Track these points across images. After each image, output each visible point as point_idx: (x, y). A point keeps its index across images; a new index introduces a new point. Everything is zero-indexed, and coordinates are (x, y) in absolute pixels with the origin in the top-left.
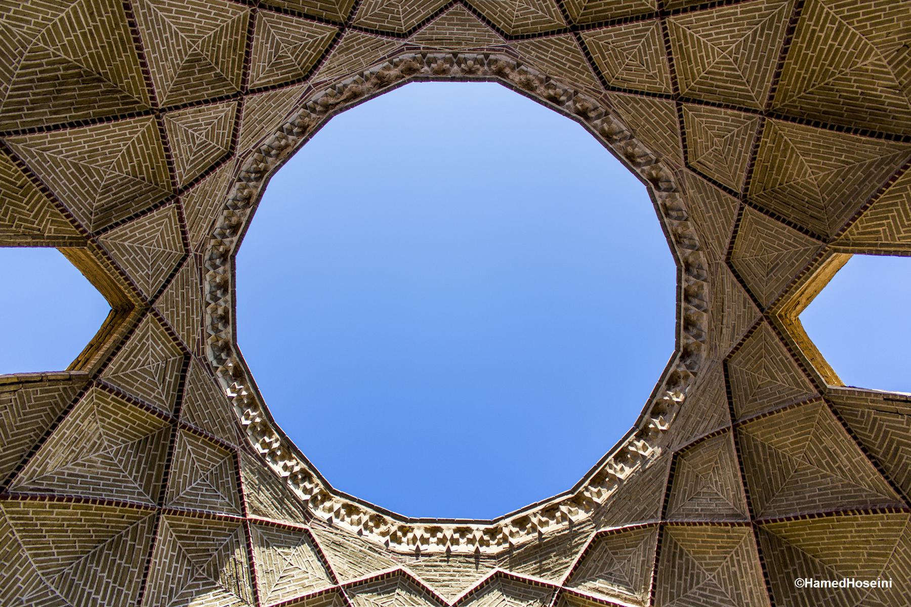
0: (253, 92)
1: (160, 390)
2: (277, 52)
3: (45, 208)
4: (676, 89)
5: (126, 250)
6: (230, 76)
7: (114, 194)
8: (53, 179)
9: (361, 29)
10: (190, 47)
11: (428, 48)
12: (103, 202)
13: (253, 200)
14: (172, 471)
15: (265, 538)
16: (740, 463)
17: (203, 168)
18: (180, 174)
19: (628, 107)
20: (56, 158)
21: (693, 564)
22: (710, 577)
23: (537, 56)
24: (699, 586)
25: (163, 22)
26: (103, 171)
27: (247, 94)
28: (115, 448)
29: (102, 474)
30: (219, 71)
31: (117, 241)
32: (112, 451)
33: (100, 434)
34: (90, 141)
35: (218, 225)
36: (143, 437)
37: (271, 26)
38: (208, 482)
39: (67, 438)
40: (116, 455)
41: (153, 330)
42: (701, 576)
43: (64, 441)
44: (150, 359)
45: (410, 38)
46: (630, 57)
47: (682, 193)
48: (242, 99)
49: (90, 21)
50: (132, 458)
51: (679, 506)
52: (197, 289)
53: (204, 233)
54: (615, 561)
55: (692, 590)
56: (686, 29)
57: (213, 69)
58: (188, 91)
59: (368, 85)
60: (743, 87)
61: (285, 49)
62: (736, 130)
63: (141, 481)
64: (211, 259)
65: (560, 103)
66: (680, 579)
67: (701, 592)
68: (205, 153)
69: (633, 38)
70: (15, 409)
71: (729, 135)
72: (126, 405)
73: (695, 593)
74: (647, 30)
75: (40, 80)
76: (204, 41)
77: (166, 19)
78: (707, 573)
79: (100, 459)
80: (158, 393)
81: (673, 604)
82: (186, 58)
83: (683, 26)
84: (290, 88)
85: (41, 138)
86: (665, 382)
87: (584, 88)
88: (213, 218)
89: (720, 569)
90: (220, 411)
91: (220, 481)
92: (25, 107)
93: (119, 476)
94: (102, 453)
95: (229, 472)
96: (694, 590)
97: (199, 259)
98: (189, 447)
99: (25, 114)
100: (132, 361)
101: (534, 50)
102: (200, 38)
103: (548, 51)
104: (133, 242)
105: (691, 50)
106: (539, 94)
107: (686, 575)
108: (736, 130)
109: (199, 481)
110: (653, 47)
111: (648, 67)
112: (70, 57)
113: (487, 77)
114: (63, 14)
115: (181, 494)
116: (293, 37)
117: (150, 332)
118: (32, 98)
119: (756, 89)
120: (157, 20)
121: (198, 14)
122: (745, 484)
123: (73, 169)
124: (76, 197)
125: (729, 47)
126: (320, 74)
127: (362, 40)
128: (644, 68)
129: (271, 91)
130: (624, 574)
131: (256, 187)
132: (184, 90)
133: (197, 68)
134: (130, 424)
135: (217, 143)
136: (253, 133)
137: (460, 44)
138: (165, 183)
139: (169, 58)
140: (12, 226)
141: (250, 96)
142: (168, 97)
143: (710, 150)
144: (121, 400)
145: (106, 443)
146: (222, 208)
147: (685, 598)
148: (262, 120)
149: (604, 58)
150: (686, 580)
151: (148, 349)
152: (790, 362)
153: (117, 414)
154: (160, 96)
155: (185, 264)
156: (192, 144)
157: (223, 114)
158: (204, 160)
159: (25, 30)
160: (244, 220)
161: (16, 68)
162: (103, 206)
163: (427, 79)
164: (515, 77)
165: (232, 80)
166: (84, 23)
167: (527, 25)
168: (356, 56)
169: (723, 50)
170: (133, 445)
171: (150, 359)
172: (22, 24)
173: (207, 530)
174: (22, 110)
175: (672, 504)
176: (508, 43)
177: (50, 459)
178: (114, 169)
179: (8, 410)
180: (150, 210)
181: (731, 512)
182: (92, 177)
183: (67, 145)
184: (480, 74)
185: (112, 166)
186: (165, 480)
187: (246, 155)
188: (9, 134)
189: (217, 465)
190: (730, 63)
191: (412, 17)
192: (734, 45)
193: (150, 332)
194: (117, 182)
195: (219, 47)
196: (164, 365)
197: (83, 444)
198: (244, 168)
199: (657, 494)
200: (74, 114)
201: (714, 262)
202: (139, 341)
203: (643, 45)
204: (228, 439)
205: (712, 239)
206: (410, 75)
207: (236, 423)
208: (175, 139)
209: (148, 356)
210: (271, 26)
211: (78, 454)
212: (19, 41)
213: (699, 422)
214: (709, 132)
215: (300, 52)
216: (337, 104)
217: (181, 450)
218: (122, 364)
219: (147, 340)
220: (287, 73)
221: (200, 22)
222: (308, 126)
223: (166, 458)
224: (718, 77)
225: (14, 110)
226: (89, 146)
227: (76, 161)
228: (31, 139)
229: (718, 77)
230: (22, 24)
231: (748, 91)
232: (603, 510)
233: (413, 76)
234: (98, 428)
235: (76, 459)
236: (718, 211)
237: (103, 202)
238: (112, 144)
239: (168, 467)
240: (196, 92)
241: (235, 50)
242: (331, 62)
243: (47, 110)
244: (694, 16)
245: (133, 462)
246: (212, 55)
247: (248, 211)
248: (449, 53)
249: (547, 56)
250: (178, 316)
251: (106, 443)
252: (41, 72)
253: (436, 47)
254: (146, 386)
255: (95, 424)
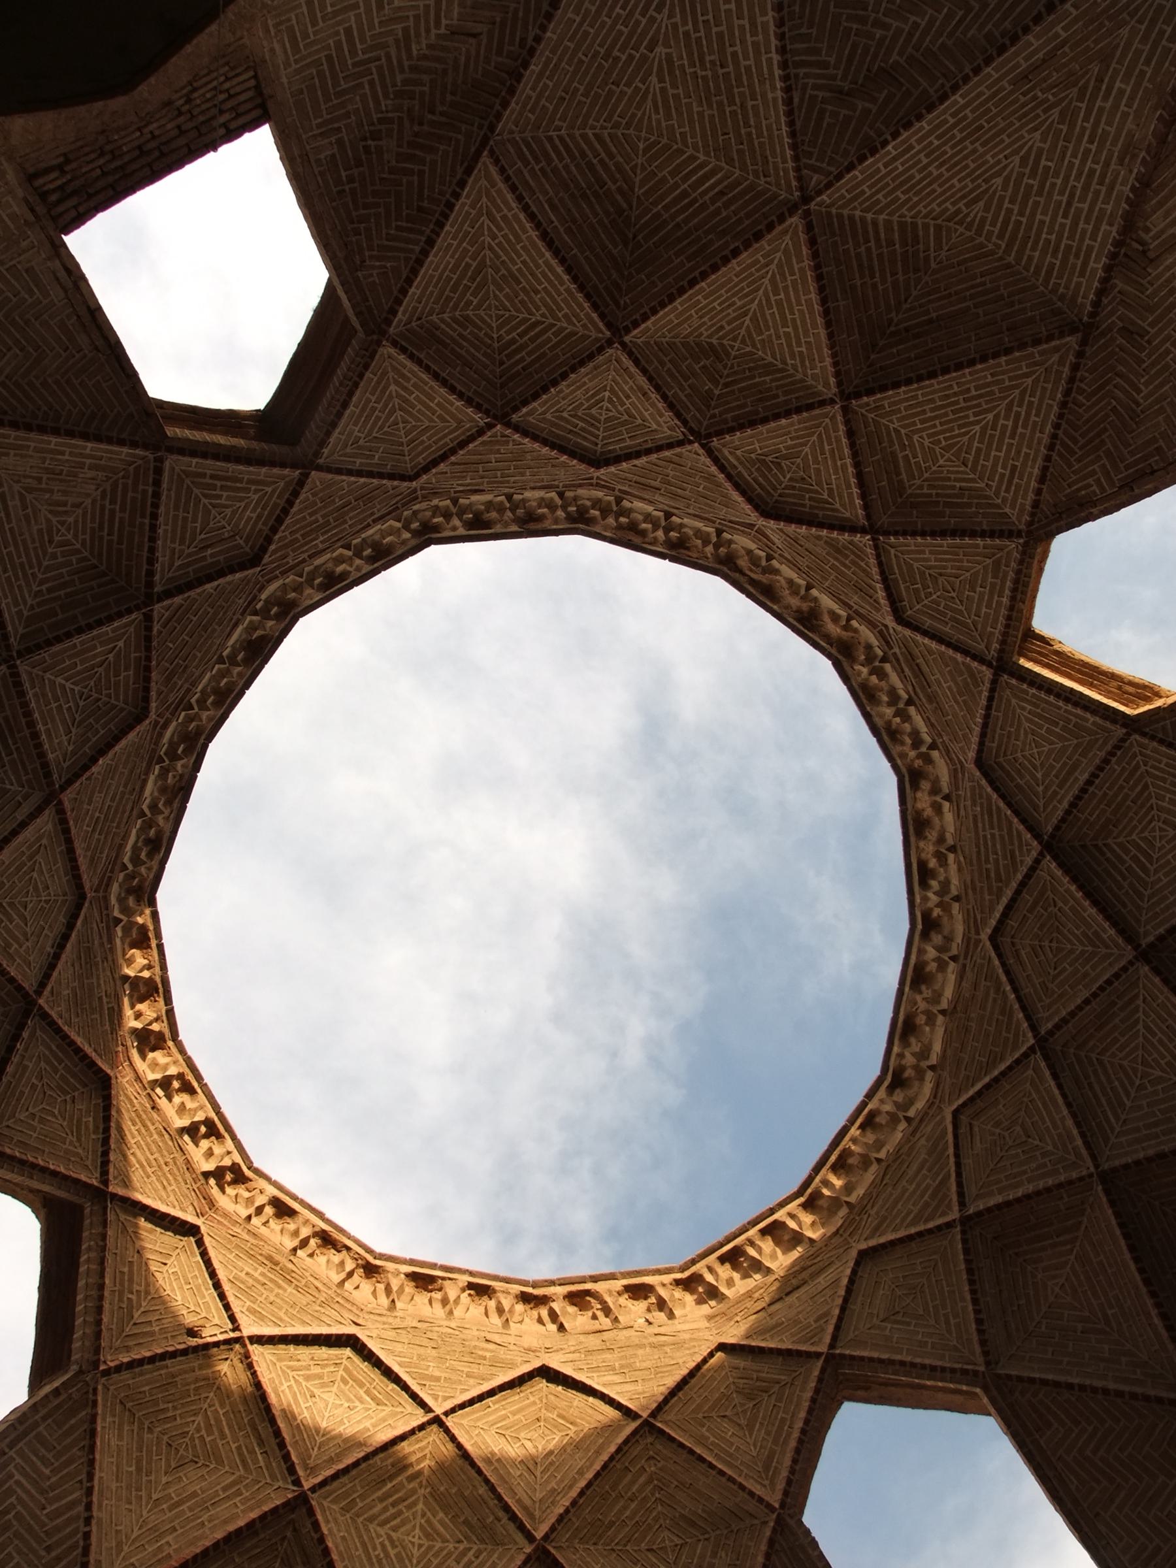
0: (710, 452)
1: (187, 551)
2: (785, 457)
3: (402, 255)
4: (1051, 1033)
5: (383, 391)
6: (716, 411)
7: (460, 335)
8: (450, 245)
9: (878, 556)
10: (735, 339)
11: (898, 660)
12: (443, 326)
13: (533, 526)
14: (76, 640)
15: (44, 841)
16: (605, 1466)
17: (558, 436)
18: (535, 409)
19: (983, 983)
20: (483, 235)
21: (415, 1504)
22: (416, 1540)
23: (975, 817)
24: (393, 1534)
25: (757, 290)
26: (490, 305)
27: (703, 446)
28: (70, 537)
29: (24, 541)
30: (717, 392)
31: (391, 374)
32: (63, 535)
33: (82, 503)
34: (528, 268)
35: (475, 498)
36: (103, 567)
37: (820, 434)
38: (81, 703)
39: (57, 460)
40: (62, 544)
41: (274, 491)
42: (408, 1527)
43: (51, 459)
44: (228, 511)
45: (899, 628)
46: (1054, 945)
47: (911, 1129)
48: (691, 442)
49: (711, 194)
50: (64, 570)
51: (479, 1424)
52: (364, 519)
53: (456, 485)
54: (334, 1389)
55: (378, 1529)
56: (1141, 997)
57: (716, 383)
58: (669, 365)
59: (794, 602)
60: (1113, 1120)
61: (794, 468)
62: (1050, 1148)
63: (39, 604)
64: (415, 513)
65: (924, 884)
66: (382, 1499)
67: (387, 1543)
68: (583, 429)
69: (1085, 934)
70: (71, 362)
71: (1037, 1142)
72: (143, 516)
73: (379, 1536)
74: (1107, 947)
75: (590, 166)
76: (751, 354)
77: (761, 292)
78: (417, 1531)
79: (44, 526)
80: (182, 551)
81: (343, 1515)
82: (714, 341)
83: (1142, 991)
84: (740, 499)
85: (506, 203)
86: (625, 1282)
87: (970, 907)
88: (485, 487)
89: (438, 1545)
90: (195, 656)
91: (91, 720)
92: (543, 163)
93: (31, 567)
94: (55, 523)
95: (112, 726)
96: (381, 1531)
97: (413, 498)
98: (121, 644)
99: (533, 168)
100: (214, 487)
101: (982, 807)
102: (754, 346)
103: (992, 828)
104: (398, 396)
105: (1117, 1021)
106: (918, 848)
107: (393, 1505)
108: (1050, 1148)
109: (76, 689)
110: (1088, 967)
111: (1055, 977)
112: (640, 188)
113: (899, 762)
114: (702, 158)
115: (48, 675)
116: (818, 471)
117: (269, 489)
118: (560, 166)
119: (1123, 1139)
120: (754, 282)
121: (790, 330)
122: (582, 1493)
123: (474, 264)
124: (435, 286)
125: (1152, 1067)
126: (781, 530)
127: (862, 564)
128: (1052, 972)
129: (722, 476)
130: (327, 1415)
131: (556, 521)
132: (666, 359)
133: (707, 363)
134: (115, 538)
135: (604, 438)
136: (642, 480)
137: (930, 700)
138: (510, 396)
139: (706, 319)
140: (352, 222)
141: (701, 451)
142: (647, 343)
143: (998, 1131)
144: (149, 503)
145: (71, 520)
146: (507, 490)
147: (361, 1526)
148: (669, 483)
149: (1030, 911)
150: (385, 1509)
151: (241, 500)
152: (789, 1435)
153: (123, 510)
154: (643, 333)
155: (396, 483)
156: (586, 405)
157: (655, 426)
158: (571, 432)
159: (654, 117)
160: (498, 529)
161: (593, 128)
162: (437, 329)
163: (845, 678)
164: (923, 801)
165: (714, 416)
166: (703, 188)
167: (1012, 780)
168: (833, 567)
169: (1144, 1063)
170: (85, 559)
171: (228, 511)
172: (661, 111)
173: (13, 747)
174: (538, 162)
175: (473, 1412)
176: (971, 766)
177: (15, 455)
178: (499, 317)
179: (64, 355)
180: (461, 396)
181: (528, 1502)
182: (474, 295)
183: (509, 241)
184: (896, 750)
185: (501, 313)
186: (59, 640)
187: (604, 486)
188: (497, 161)
189: (113, 701)
190: (1132, 1084)
191: (932, 617)
192: (1161, 1073)
193: (269, 489)
194: (480, 329)
195: (754, 377)
196: (226, 535)
197: (56, 488)
198: (581, 492)
199: (472, 1381)
200: (562, 230)
201: (846, 1235)
202: (250, 482)
203: (1083, 952)
204: (159, 693)
205: (877, 1213)
206: (839, 652)
207: (188, 690)
208: (586, 379)
209: (231, 506)
210: (820, 434)
211: (41, 490)
212: (634, 115)
213: (614, 1369)
214: (1022, 1113)
215: (801, 489)
216: (744, 574)
217: (111, 635)
218: (204, 475)
219: (256, 491)
220: (760, 485)
221: (779, 337)
222: (688, 549)
223: (91, 621)
224: (1103, 1078)
225: (532, 152)
226: (519, 270)
227: (488, 263)
228: (499, 192)
229: (1103, 1078)
230: (661, 111)
231: (1112, 1129)
232: (390, 1320)
233: (840, 657)
234: (88, 495)
235: (29, 490)
236: (922, 1196)
237: (443, 326)
238: (537, 298)
239: (80, 631)
240: (671, 375)
241: (760, 400)
242: (806, 538)
243: (551, 193)
244: (1166, 998)
245: (61, 576)
246: (735, 373)
247: (514, 528)
248: (908, 693)
249: (984, 830)
250: (311, 515)
251: (71, 520)
252: (601, 161)
253: (906, 670)
254: (184, 528)
255: (93, 487)
